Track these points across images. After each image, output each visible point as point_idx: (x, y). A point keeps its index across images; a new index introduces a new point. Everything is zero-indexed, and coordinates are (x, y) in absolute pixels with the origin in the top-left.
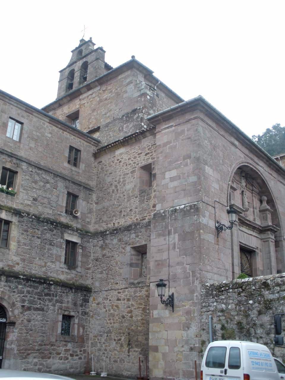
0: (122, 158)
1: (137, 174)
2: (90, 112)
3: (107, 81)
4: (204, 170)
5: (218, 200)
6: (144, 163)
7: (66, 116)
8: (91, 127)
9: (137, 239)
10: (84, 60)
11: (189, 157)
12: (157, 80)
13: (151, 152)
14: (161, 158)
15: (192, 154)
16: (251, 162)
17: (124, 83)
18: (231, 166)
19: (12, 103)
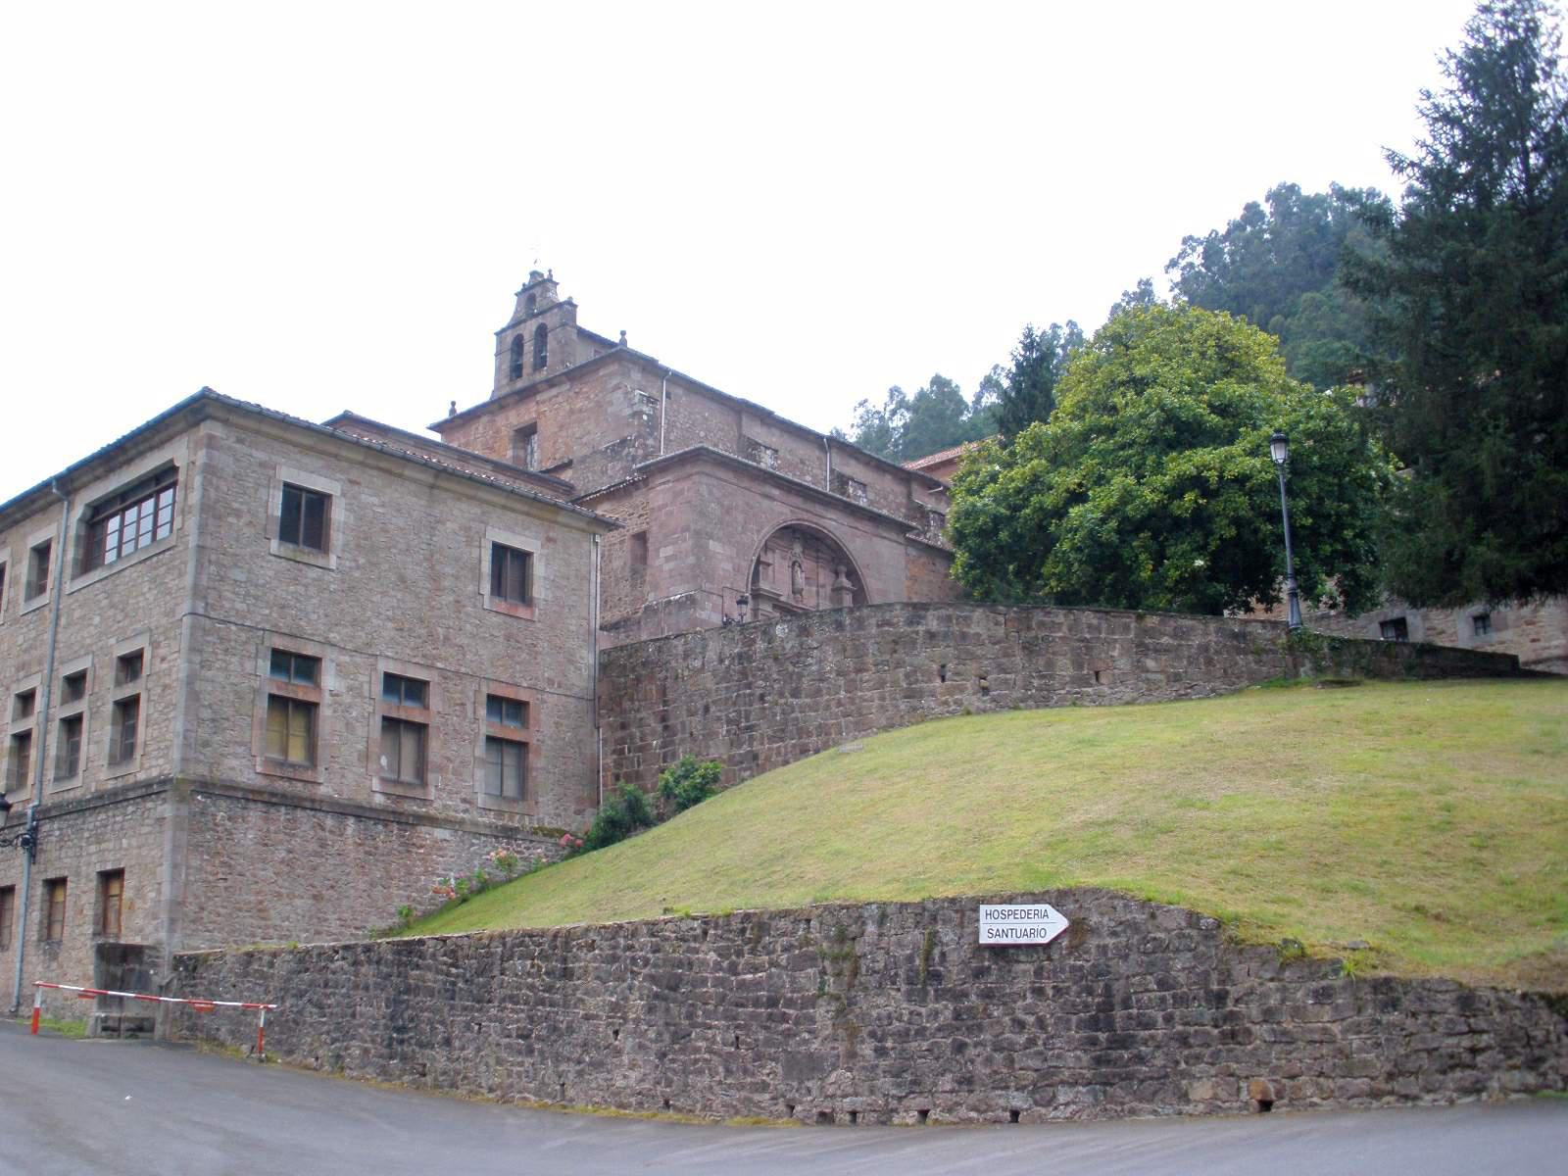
1: (627, 545)
4: (707, 547)
6: (636, 530)
8: (561, 457)
10: (540, 320)
11: (686, 529)
12: (666, 371)
16: (806, 516)
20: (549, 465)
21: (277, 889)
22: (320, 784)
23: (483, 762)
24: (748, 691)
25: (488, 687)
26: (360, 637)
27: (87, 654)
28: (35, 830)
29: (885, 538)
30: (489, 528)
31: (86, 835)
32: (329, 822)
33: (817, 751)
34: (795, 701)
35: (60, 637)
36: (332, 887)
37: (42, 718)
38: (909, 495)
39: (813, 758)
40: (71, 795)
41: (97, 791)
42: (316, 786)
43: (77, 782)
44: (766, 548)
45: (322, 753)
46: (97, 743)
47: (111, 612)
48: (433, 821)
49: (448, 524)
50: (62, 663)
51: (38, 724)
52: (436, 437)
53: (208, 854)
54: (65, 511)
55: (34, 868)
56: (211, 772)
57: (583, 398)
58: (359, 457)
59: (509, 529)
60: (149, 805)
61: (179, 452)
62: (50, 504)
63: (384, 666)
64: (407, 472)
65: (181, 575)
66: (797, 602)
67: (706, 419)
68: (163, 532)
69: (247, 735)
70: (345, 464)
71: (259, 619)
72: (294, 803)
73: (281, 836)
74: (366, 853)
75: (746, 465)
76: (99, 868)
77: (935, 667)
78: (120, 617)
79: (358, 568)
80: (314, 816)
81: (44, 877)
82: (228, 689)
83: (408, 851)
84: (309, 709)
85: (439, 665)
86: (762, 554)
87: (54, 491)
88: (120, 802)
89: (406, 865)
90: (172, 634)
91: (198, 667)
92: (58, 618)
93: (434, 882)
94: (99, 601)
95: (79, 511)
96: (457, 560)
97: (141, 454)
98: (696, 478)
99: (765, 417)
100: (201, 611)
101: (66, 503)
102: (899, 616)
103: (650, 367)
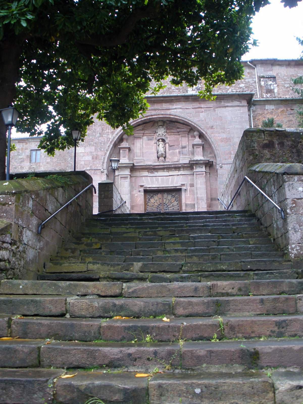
19: (30, 141)
29: (227, 106)
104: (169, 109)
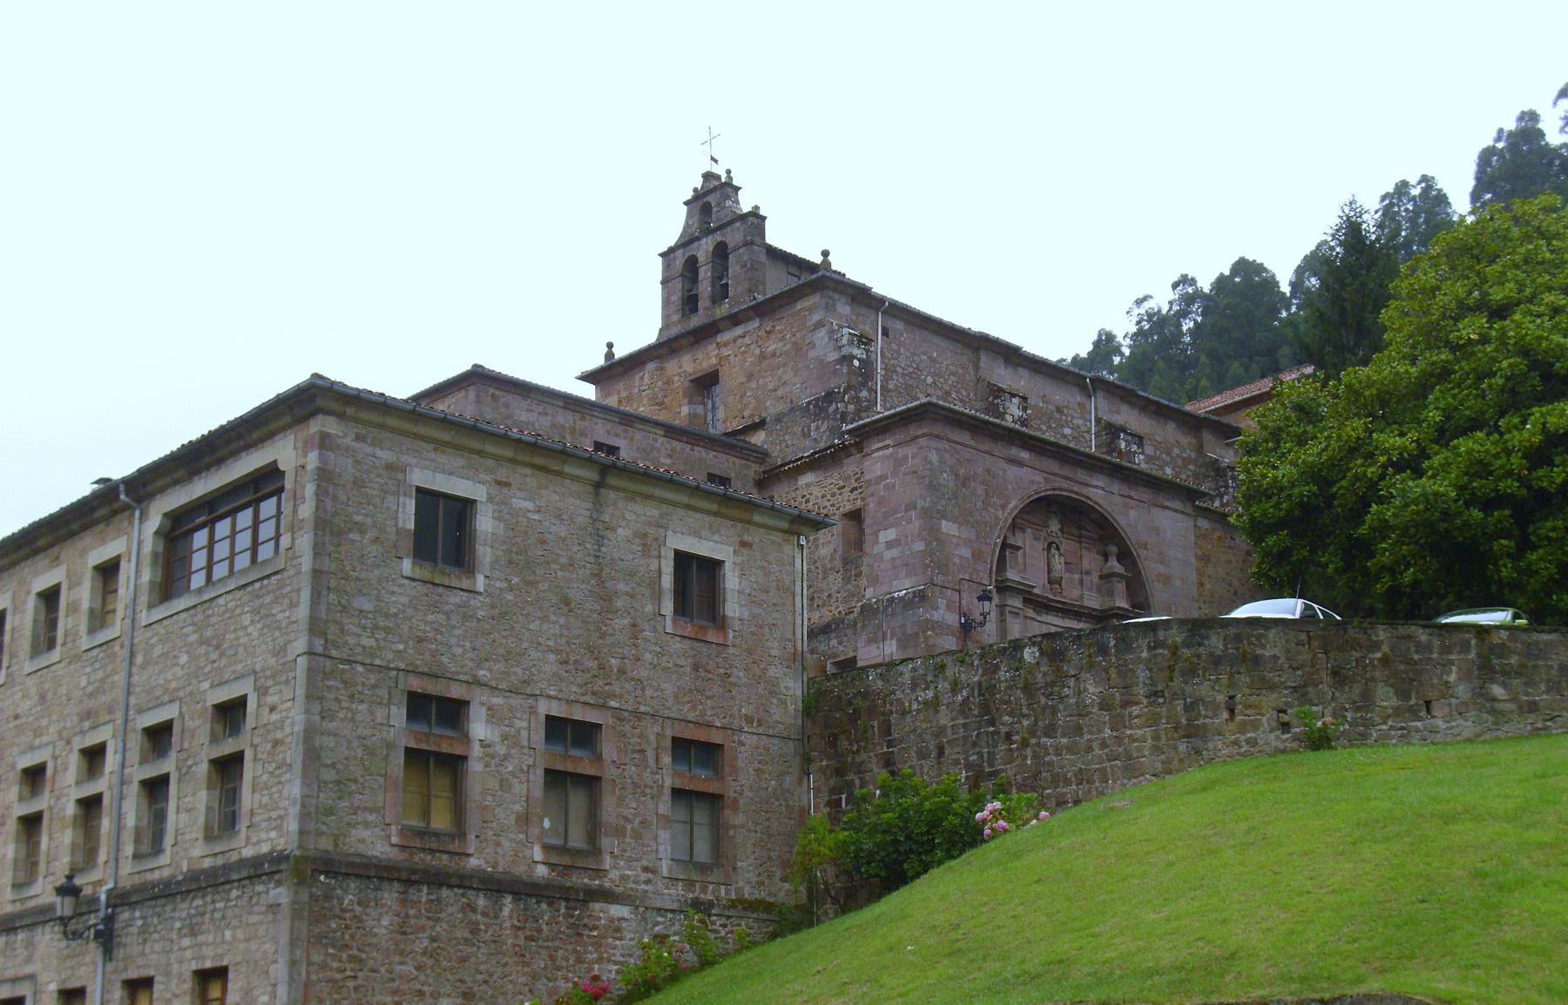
0: (811, 494)
2: (742, 379)
3: (774, 310)
4: (939, 529)
5: (967, 577)
6: (849, 507)
7: (692, 381)
8: (749, 415)
9: (841, 648)
10: (718, 237)
12: (881, 300)
13: (861, 487)
14: (872, 505)
15: (918, 502)
16: (1064, 484)
17: (809, 324)
18: (1003, 507)
19: (595, 413)
20: (736, 425)
21: (419, 987)
22: (469, 855)
23: (667, 821)
24: (991, 729)
25: (673, 727)
26: (515, 673)
27: (171, 701)
28: (109, 920)
29: (1168, 508)
30: (670, 533)
31: (178, 925)
32: (481, 902)
33: (1077, 802)
34: (1049, 742)
35: (136, 679)
36: (486, 982)
37: (115, 780)
38: (1200, 449)
39: (1074, 812)
40: (156, 875)
41: (189, 870)
42: (464, 858)
43: (164, 859)
44: (1014, 527)
45: (473, 819)
46: (188, 811)
47: (203, 649)
48: (608, 896)
49: (620, 531)
50: (140, 712)
51: (110, 788)
52: (588, 392)
53: (334, 946)
54: (137, 522)
55: (110, 967)
56: (336, 845)
57: (777, 338)
58: (509, 453)
59: (696, 534)
60: (260, 888)
61: (284, 452)
62: (115, 513)
63: (544, 708)
64: (567, 469)
65: (293, 605)
66: (1054, 594)
67: (934, 361)
68: (265, 552)
69: (381, 798)
70: (491, 463)
71: (390, 656)
72: (438, 880)
73: (423, 921)
74: (527, 938)
75: (987, 422)
76: (194, 966)
77: (1221, 698)
78: (214, 656)
79: (511, 589)
80: (463, 895)
81: (124, 976)
82: (355, 744)
83: (579, 935)
84: (454, 764)
85: (613, 704)
86: (1010, 536)
87: (122, 497)
88: (222, 884)
89: (575, 951)
90: (283, 678)
91: (318, 718)
92: (132, 655)
93: (610, 971)
94: (187, 635)
95: (154, 522)
96: (632, 574)
97: (234, 454)
98: (922, 441)
99: (1011, 355)
100: (320, 650)
101: (137, 513)
102: (1176, 636)
103: (861, 296)
104: (1087, 485)
